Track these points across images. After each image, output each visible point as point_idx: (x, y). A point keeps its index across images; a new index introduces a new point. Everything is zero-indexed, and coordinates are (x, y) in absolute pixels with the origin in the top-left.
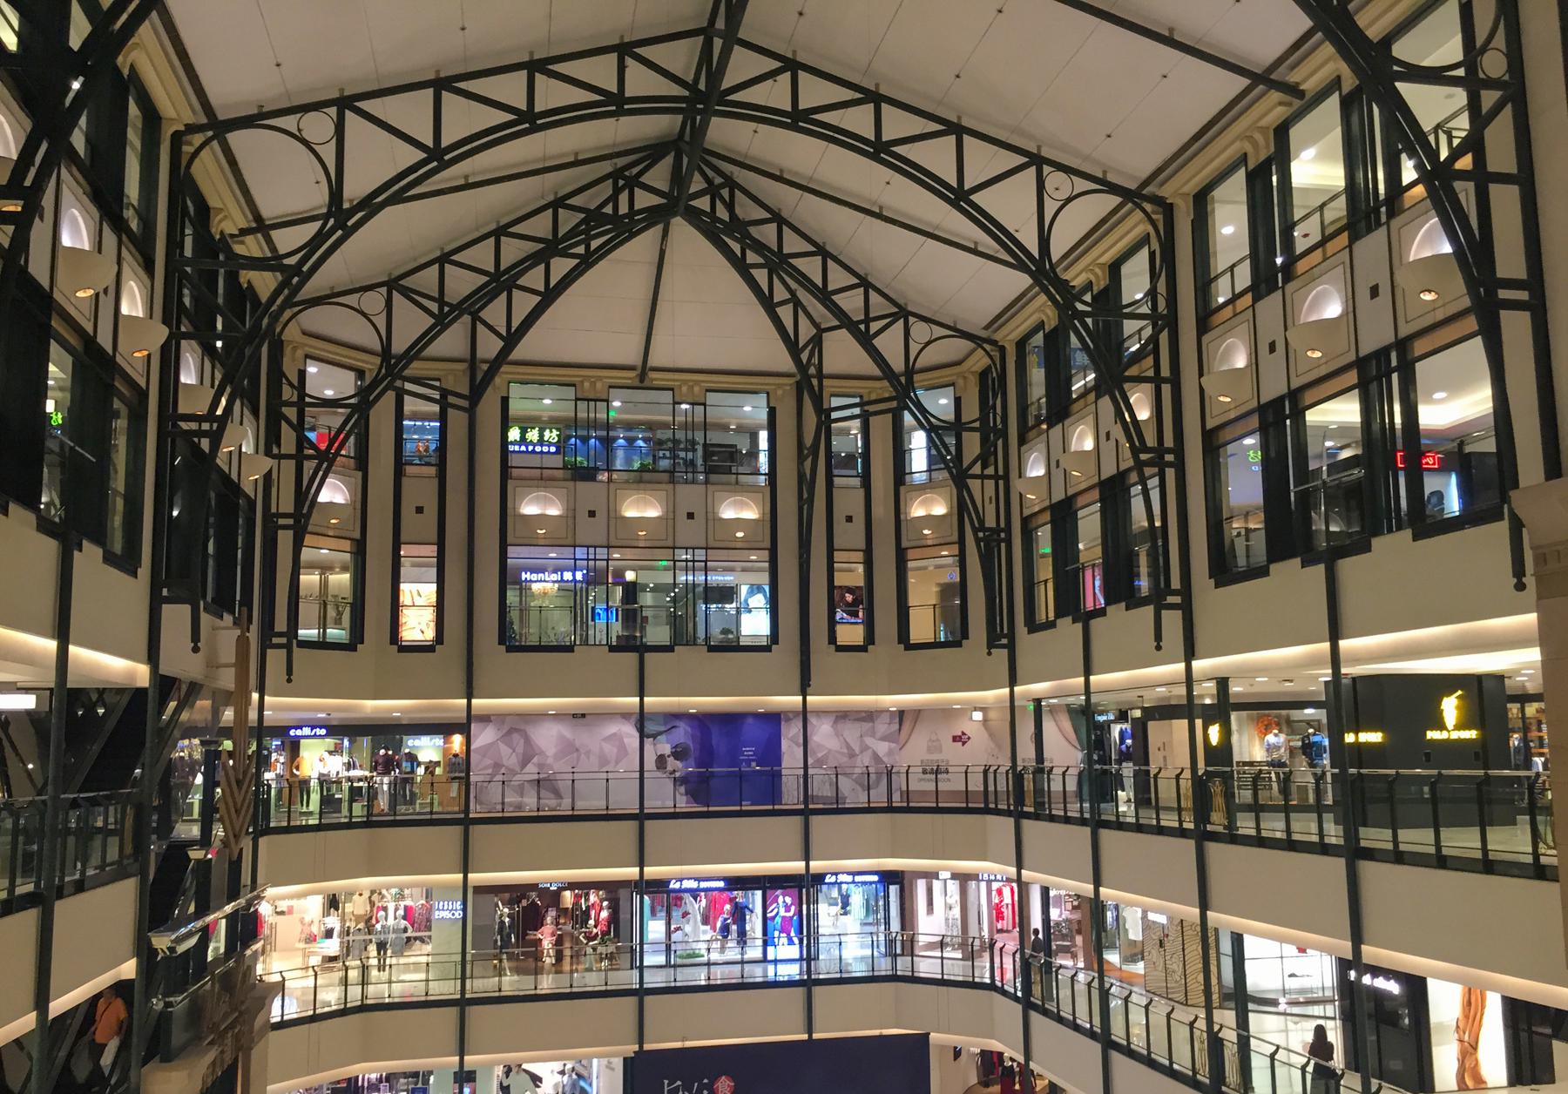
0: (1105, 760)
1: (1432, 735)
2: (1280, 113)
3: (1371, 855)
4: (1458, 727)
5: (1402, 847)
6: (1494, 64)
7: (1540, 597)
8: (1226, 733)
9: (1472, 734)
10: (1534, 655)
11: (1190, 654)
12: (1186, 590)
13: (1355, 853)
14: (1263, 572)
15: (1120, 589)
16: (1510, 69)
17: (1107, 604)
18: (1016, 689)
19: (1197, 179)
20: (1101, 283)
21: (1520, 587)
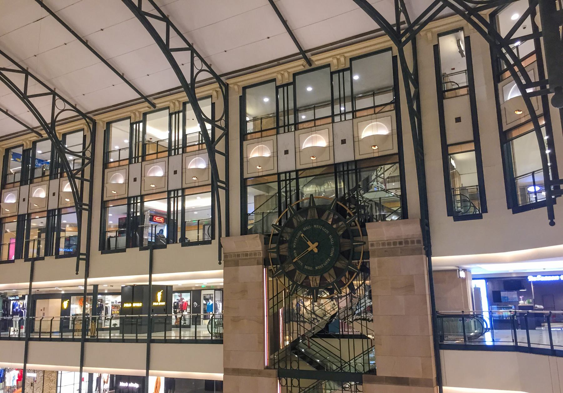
0: (8, 315)
1: (155, 304)
2: (147, 109)
3: (154, 341)
4: (161, 301)
5: (555, 348)
6: (88, 154)
7: (225, 266)
8: (69, 304)
9: (164, 303)
10: (222, 280)
11: (87, 276)
12: (88, 254)
13: (150, 341)
14: (124, 250)
15: (51, 250)
16: (91, 156)
17: (16, 258)
18: (33, 283)
19: (16, 143)
20: (30, 146)
21: (220, 263)
